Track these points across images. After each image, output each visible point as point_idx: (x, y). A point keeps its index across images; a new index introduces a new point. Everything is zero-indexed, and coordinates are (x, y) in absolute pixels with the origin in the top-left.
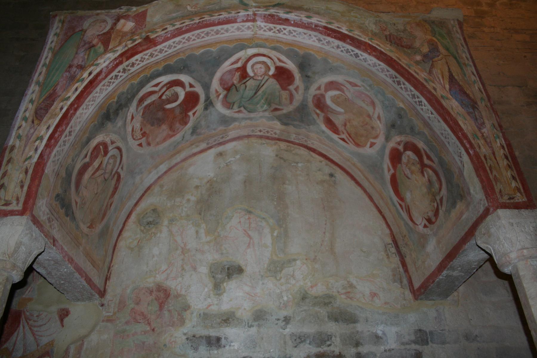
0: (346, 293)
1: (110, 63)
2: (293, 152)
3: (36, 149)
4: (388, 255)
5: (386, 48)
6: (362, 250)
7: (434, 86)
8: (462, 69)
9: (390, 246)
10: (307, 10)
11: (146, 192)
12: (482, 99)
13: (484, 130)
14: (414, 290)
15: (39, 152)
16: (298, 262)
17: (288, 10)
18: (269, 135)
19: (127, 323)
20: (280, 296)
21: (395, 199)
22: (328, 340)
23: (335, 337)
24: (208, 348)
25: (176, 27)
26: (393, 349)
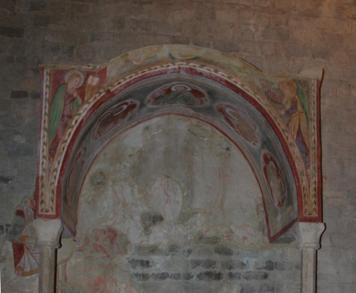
0: (227, 236)
1: (87, 113)
2: (202, 128)
3: (55, 178)
4: (258, 212)
5: (263, 102)
6: (242, 208)
7: (288, 136)
8: (307, 121)
9: (261, 206)
10: (216, 64)
11: (94, 160)
13: (308, 170)
14: (270, 238)
15: (57, 179)
16: (199, 215)
17: (202, 63)
18: (184, 114)
19: (92, 252)
20: (186, 237)
21: (266, 180)
22: (213, 265)
23: (218, 263)
24: (142, 267)
26: (251, 272)
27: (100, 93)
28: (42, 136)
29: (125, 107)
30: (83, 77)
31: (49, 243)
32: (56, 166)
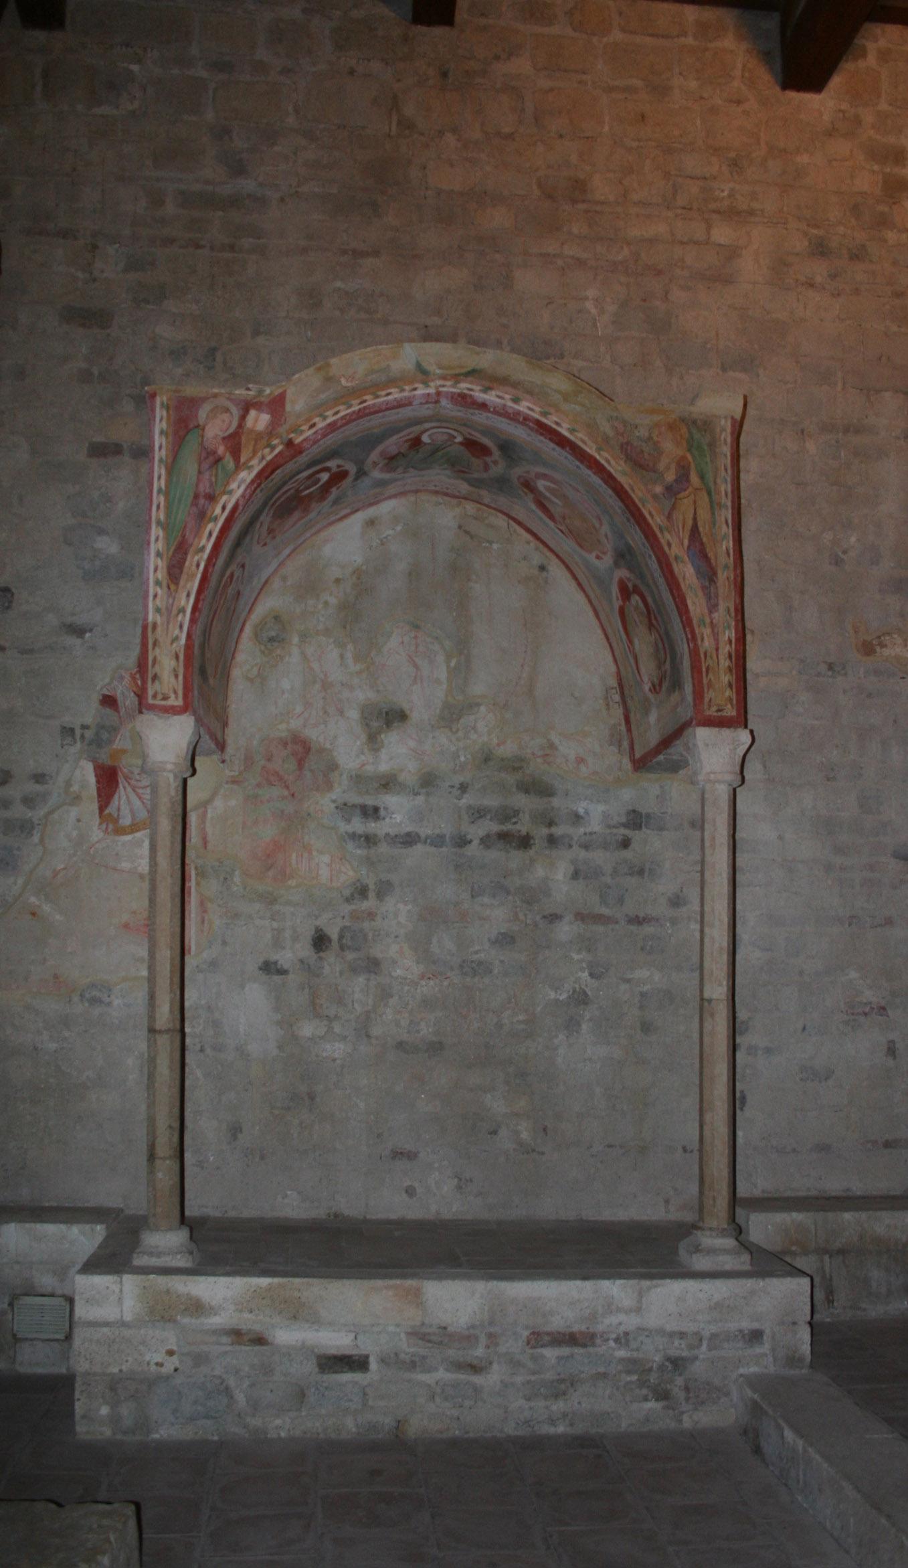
3: (181, 627)
4: (608, 705)
6: (572, 695)
12: (726, 567)
13: (715, 615)
16: (483, 709)
19: (259, 785)
20: (456, 756)
25: (329, 421)
27: (273, 448)
28: (153, 538)
29: (325, 477)
30: (236, 412)
31: (169, 767)
32: (183, 603)
